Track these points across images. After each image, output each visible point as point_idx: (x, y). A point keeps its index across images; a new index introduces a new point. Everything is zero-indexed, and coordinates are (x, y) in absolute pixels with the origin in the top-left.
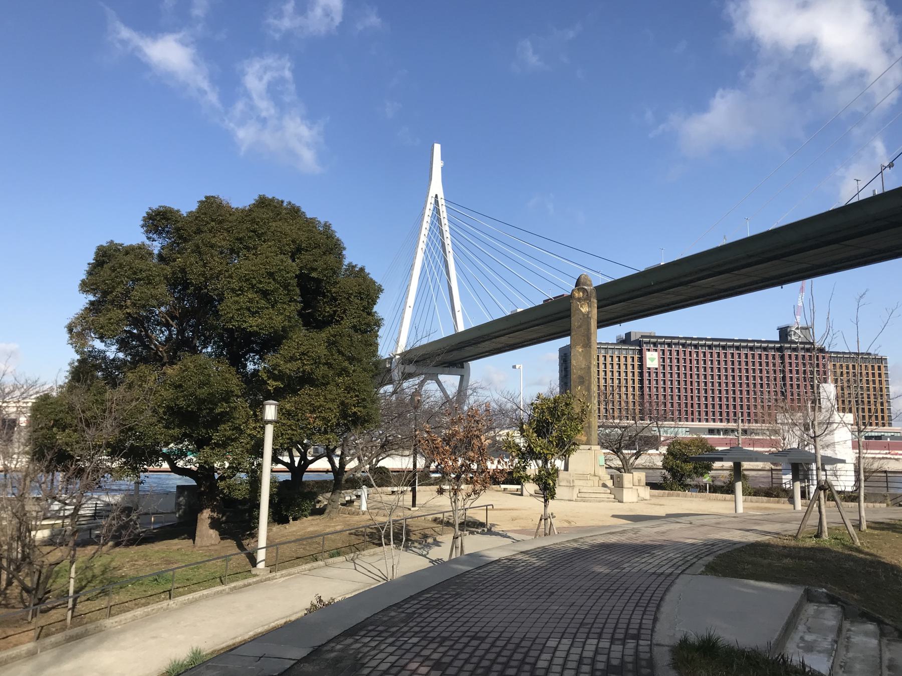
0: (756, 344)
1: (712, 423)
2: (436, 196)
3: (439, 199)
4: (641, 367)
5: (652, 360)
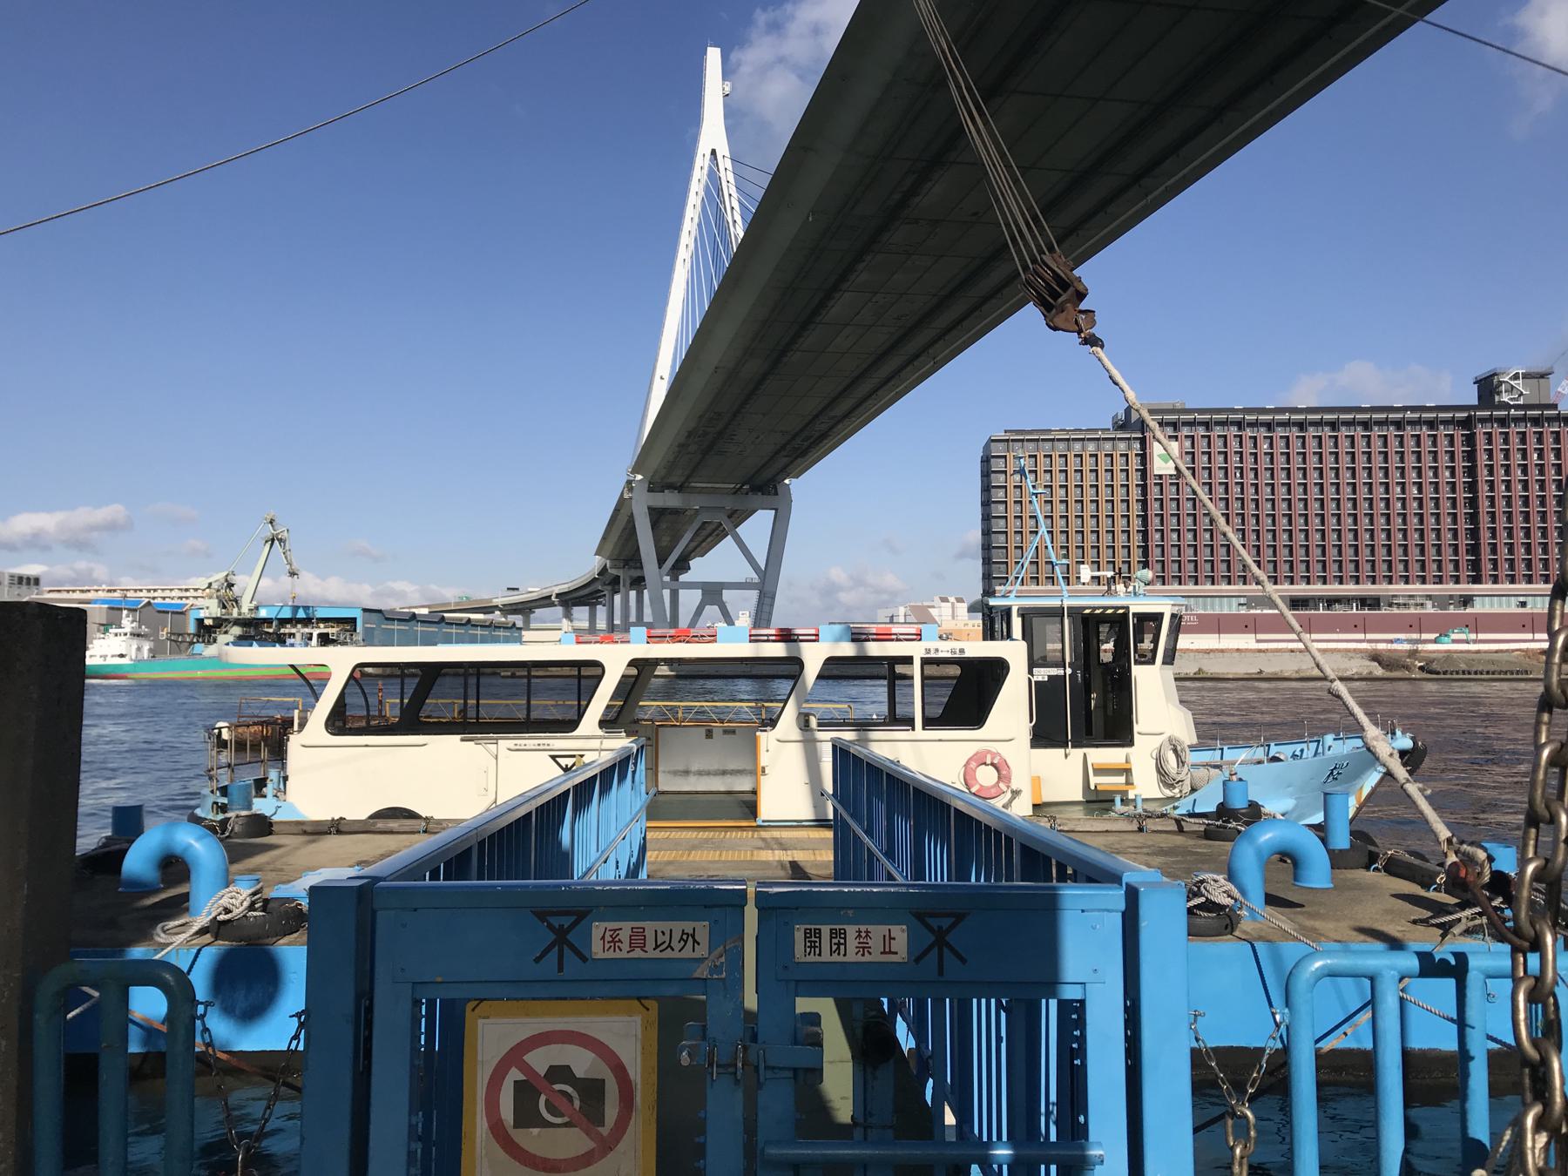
0: (1409, 415)
1: (1304, 586)
2: (714, 152)
4: (1144, 473)
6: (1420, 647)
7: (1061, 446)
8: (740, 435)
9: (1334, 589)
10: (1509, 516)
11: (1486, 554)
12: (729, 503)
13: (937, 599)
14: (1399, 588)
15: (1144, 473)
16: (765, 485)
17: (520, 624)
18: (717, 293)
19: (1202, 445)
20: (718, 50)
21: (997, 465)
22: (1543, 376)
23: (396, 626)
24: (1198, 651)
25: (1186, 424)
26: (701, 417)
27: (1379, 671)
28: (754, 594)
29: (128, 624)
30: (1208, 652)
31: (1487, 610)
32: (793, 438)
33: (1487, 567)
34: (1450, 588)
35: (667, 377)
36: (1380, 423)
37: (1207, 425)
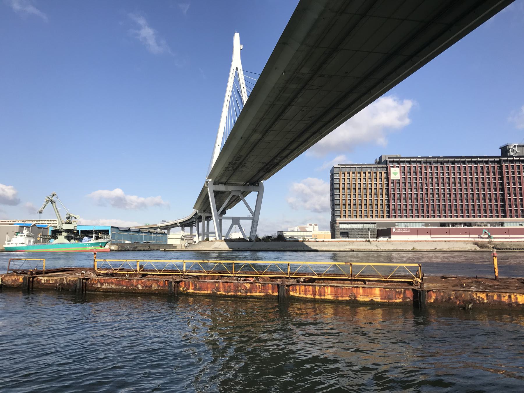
0: (479, 159)
2: (237, 69)
3: (239, 71)
4: (387, 179)
5: (395, 174)
7: (358, 169)
8: (253, 158)
9: (454, 220)
10: (515, 194)
11: (508, 208)
12: (242, 189)
13: (308, 224)
14: (477, 219)
15: (387, 179)
16: (254, 183)
17: (166, 233)
18: (237, 121)
19: (407, 170)
21: (336, 176)
23: (123, 233)
24: (411, 241)
25: (402, 162)
26: (234, 157)
27: (478, 249)
28: (250, 221)
29: (25, 232)
30: (415, 242)
32: (267, 165)
33: (508, 213)
34: (495, 219)
35: (220, 145)
36: (469, 162)
37: (409, 162)
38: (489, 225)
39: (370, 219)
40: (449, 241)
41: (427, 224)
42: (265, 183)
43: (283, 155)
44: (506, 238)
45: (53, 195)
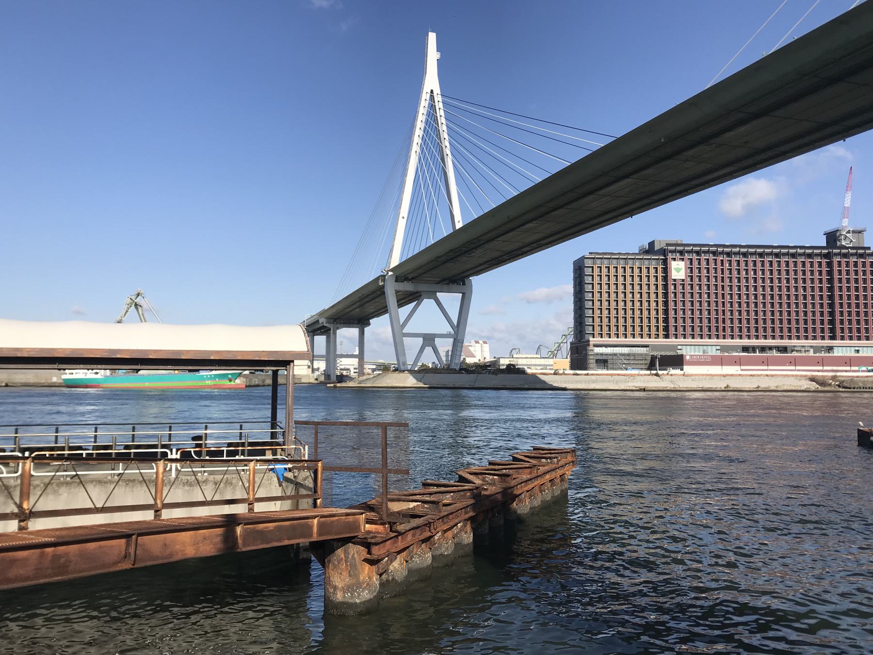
0: (799, 251)
2: (432, 91)
3: (435, 94)
4: (665, 279)
5: (678, 270)
6: (839, 374)
9: (762, 342)
10: (772, 304)
11: (838, 326)
13: (473, 342)
14: (794, 342)
15: (665, 279)
20: (434, 34)
22: (860, 232)
28: (452, 340)
31: (865, 354)
33: (838, 333)
34: (818, 342)
38: (812, 350)
39: (638, 340)
40: (772, 376)
41: (723, 349)
42: (478, 282)
43: (543, 242)
44: (819, 371)
45: (138, 295)
